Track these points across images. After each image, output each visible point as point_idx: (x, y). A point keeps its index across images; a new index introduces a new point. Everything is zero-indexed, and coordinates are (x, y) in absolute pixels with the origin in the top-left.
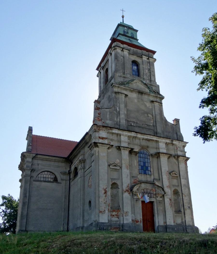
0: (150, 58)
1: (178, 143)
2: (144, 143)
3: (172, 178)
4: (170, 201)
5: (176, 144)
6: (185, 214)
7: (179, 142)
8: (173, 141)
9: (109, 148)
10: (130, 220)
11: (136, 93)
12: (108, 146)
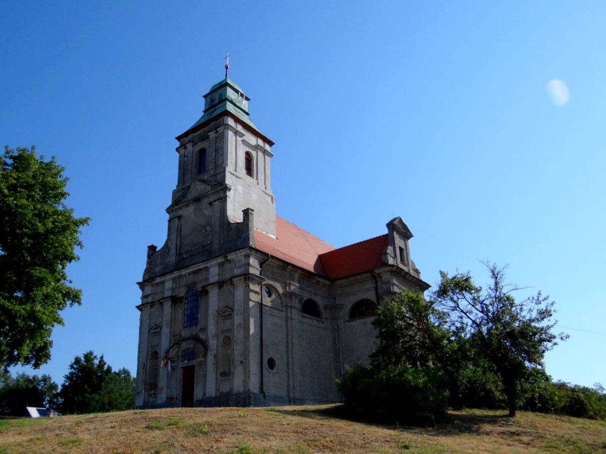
0: (218, 130)
1: (235, 256)
2: (190, 279)
4: (214, 358)
5: (232, 258)
6: (147, 357)
7: (237, 254)
8: (227, 256)
9: (151, 307)
12: (149, 305)
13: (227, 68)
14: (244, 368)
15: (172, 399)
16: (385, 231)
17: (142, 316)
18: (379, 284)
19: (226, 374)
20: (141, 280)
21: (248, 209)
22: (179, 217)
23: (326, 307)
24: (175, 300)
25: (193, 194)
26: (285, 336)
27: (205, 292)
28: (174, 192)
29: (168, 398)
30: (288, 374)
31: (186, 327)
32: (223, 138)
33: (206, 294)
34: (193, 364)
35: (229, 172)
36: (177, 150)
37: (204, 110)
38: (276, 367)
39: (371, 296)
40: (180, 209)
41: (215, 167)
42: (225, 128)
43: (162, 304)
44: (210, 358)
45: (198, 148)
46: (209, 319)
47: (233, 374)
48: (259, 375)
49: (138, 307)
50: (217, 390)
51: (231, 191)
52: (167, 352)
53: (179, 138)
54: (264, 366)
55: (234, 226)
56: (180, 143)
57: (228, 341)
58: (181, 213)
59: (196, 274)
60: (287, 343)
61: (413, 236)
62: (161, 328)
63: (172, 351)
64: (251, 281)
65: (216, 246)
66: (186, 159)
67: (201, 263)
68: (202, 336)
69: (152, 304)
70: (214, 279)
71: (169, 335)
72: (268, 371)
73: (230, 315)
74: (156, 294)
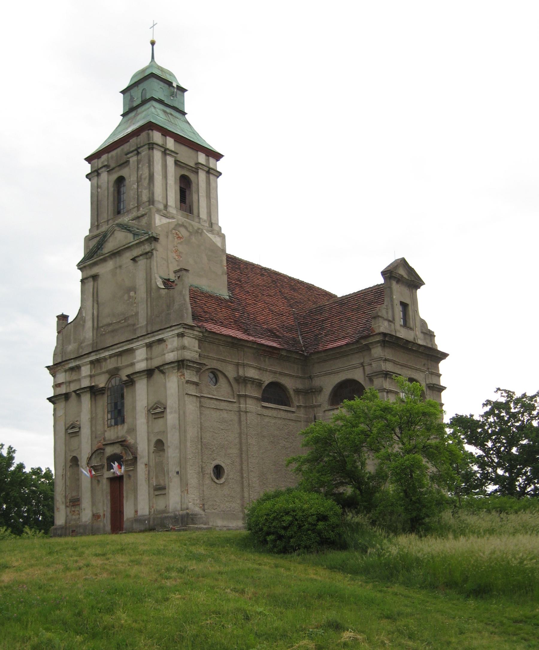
0: (139, 150)
2: (111, 364)
4: (146, 467)
13: (153, 43)
16: (381, 280)
17: (55, 410)
20: (51, 363)
22: (95, 277)
23: (297, 392)
25: (110, 246)
26: (237, 435)
27: (131, 381)
28: (88, 239)
29: (94, 515)
33: (132, 385)
36: (88, 176)
37: (122, 113)
38: (225, 476)
40: (95, 264)
41: (166, 149)
43: (79, 395)
45: (115, 176)
46: (137, 417)
47: (169, 488)
49: (50, 399)
52: (90, 459)
53: (89, 159)
55: (164, 293)
56: (92, 168)
57: (160, 445)
59: (119, 359)
60: (241, 443)
61: (424, 284)
62: (80, 428)
63: (95, 458)
64: (186, 369)
66: (99, 190)
68: (130, 440)
70: (141, 366)
71: (90, 438)
72: (214, 482)
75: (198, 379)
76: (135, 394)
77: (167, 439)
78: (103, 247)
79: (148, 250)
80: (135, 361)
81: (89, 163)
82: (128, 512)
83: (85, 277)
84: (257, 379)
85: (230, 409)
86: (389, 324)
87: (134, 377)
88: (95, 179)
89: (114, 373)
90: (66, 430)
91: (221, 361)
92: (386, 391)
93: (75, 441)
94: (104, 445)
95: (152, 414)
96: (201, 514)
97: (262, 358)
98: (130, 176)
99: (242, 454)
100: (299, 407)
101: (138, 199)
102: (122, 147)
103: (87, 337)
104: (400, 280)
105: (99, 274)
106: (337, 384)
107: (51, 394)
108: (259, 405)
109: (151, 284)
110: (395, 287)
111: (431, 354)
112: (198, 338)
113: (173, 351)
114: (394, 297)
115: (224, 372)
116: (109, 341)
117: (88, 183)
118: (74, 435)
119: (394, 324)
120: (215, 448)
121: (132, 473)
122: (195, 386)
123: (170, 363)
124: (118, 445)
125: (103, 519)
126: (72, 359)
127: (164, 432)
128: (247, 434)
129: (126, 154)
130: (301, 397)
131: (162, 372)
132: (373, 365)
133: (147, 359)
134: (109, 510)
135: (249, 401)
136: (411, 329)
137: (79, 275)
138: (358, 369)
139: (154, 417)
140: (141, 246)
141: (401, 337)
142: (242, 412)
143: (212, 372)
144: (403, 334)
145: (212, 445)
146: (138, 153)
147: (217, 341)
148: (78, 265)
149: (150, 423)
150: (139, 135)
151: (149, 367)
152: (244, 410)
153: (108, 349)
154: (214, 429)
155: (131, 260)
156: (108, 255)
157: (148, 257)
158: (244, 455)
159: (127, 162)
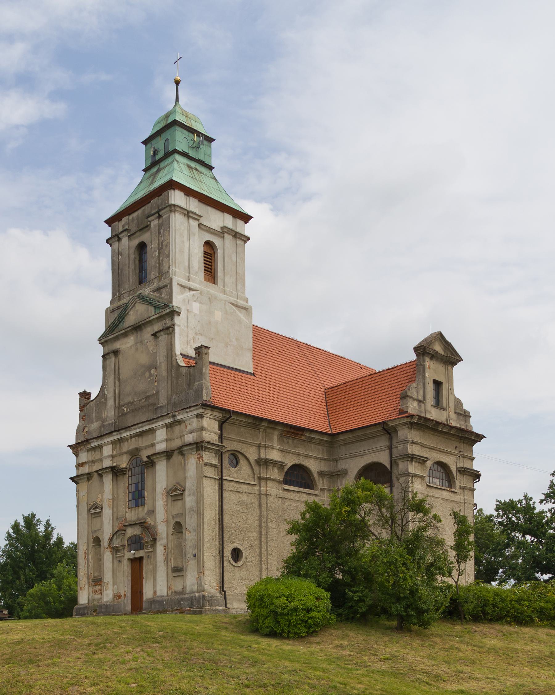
3: (174, 500)
4: (165, 549)
10: (111, 596)
11: (133, 333)
12: (86, 476)
13: (177, 83)
14: (198, 562)
15: (120, 597)
17: (78, 491)
18: (394, 441)
19: (178, 571)
20: (73, 442)
21: (201, 347)
23: (321, 474)
24: (116, 472)
25: (131, 319)
26: (257, 518)
27: (151, 463)
28: (109, 312)
29: (115, 595)
30: (261, 567)
31: (132, 508)
32: (169, 228)
34: (141, 555)
35: (178, 284)
36: (108, 241)
37: (144, 168)
38: (243, 559)
39: (383, 458)
40: (117, 338)
42: (171, 211)
43: (100, 476)
44: (160, 549)
45: (136, 242)
47: (186, 570)
48: (218, 571)
49: (72, 479)
50: (169, 588)
51: (181, 315)
52: (111, 539)
53: (109, 222)
54: (225, 559)
57: (178, 527)
58: (117, 345)
59: (140, 439)
60: (260, 526)
61: (460, 360)
62: (102, 509)
63: (117, 538)
65: (163, 401)
67: (145, 424)
68: (150, 521)
69: (89, 476)
70: (161, 447)
71: (112, 518)
72: (232, 564)
73: (182, 494)
74: (93, 462)
75: (217, 462)
76: (155, 475)
77: (185, 522)
78: (124, 320)
79: (169, 325)
80: (155, 441)
81: (110, 226)
82: (148, 593)
83: (107, 352)
84: (279, 462)
85: (250, 492)
86: (418, 404)
87: (155, 459)
88: (116, 245)
89: (134, 453)
90: (89, 510)
91: (242, 443)
92: (411, 475)
93: (97, 520)
94: (125, 526)
95: (171, 496)
96: (216, 596)
97: (285, 439)
98: (151, 242)
99: (261, 537)
100: (322, 490)
101: (159, 268)
102: (143, 208)
103: (109, 415)
104: (434, 356)
105: (120, 349)
106: (363, 467)
107: (74, 474)
108: (280, 488)
109: (172, 362)
110: (428, 362)
111: (464, 436)
112: (218, 419)
113: (192, 433)
114: (427, 375)
115: (245, 453)
116: (130, 422)
117: (108, 248)
118: (96, 516)
119: (425, 404)
120: (233, 531)
121: (152, 554)
122: (213, 468)
123: (188, 444)
124: (138, 527)
125: (123, 599)
126: (94, 438)
127: (182, 515)
128: (267, 517)
129: (148, 217)
130: (325, 480)
131: (182, 453)
132: (399, 448)
133: (167, 440)
134: (130, 591)
135: (270, 484)
136: (444, 409)
137: (100, 350)
138: (384, 452)
139: (173, 499)
140: (162, 320)
141: (432, 418)
142: (263, 494)
143: (233, 454)
144: (434, 414)
145: (231, 528)
146: (160, 216)
147: (238, 422)
148: (100, 340)
149: (169, 505)
150: (161, 195)
151: (169, 448)
152: (265, 493)
153: (129, 429)
154: (232, 512)
155: (152, 335)
156: (129, 329)
157: (168, 332)
158: (263, 539)
159: (148, 227)
